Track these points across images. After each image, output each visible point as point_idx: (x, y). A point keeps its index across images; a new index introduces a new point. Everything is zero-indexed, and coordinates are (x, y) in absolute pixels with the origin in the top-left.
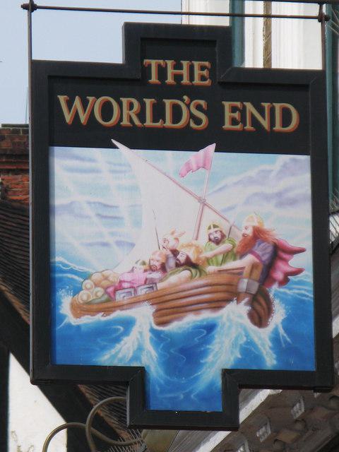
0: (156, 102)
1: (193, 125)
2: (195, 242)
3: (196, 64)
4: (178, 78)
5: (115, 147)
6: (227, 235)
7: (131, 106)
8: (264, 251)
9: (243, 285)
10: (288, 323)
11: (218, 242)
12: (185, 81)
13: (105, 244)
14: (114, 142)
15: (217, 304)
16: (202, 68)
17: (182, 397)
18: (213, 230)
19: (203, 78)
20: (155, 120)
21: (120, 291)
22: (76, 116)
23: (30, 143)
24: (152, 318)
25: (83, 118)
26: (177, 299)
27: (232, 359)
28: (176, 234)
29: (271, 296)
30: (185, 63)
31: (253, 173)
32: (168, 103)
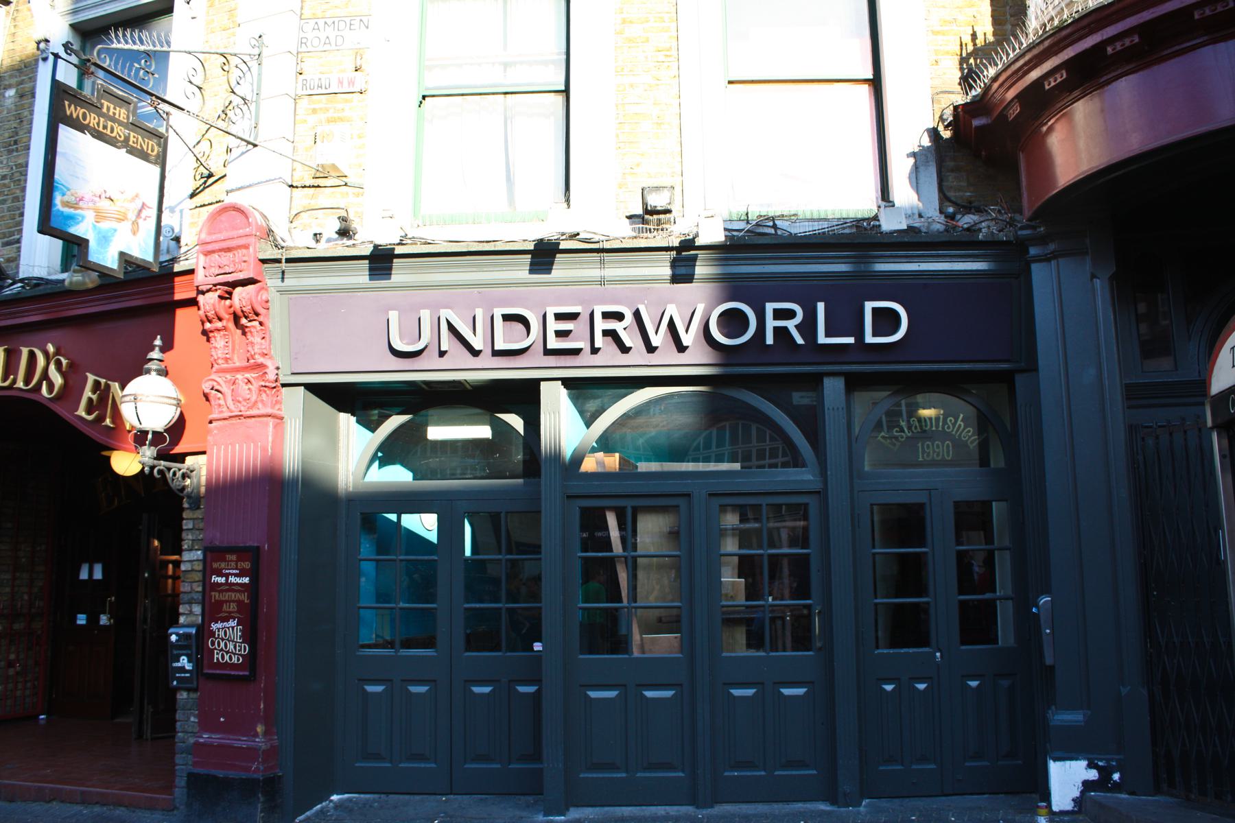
1: (118, 137)
4: (114, 114)
25: (75, 116)
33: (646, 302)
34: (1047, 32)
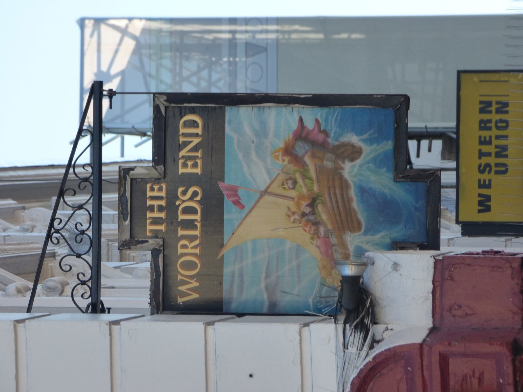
0: (181, 227)
1: (198, 198)
2: (296, 200)
3: (149, 194)
4: (161, 209)
5: (223, 256)
6: (289, 176)
7: (184, 246)
8: (301, 149)
9: (328, 164)
10: (359, 133)
11: (295, 182)
12: (163, 203)
13: (299, 266)
14: (219, 257)
15: (344, 185)
16: (152, 189)
17: (418, 213)
18: (286, 186)
19: (161, 189)
20: (195, 227)
21: (335, 257)
22: (193, 290)
24: (355, 234)
25: (195, 284)
26: (340, 215)
27: (387, 175)
28: (290, 214)
29: (337, 143)
30: (149, 203)
31: (240, 156)
32: (181, 217)
33: (350, 324)
34: (368, 314)
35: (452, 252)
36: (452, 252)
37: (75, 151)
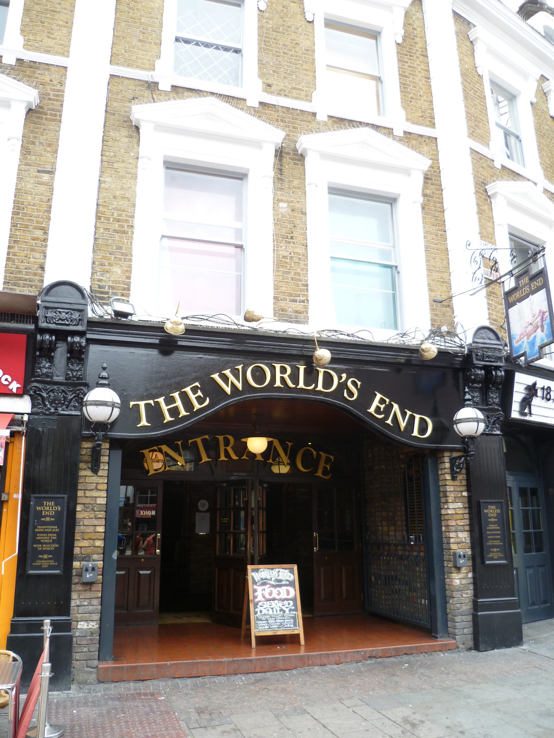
3: (188, 390)
7: (283, 370)
12: (183, 413)
15: (535, 331)
23: (262, 657)
35: (507, 154)
36: (507, 154)
37: (543, 378)
